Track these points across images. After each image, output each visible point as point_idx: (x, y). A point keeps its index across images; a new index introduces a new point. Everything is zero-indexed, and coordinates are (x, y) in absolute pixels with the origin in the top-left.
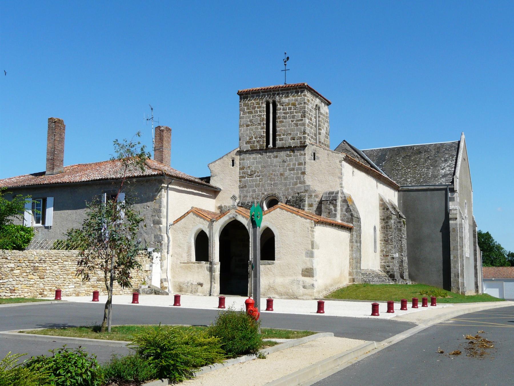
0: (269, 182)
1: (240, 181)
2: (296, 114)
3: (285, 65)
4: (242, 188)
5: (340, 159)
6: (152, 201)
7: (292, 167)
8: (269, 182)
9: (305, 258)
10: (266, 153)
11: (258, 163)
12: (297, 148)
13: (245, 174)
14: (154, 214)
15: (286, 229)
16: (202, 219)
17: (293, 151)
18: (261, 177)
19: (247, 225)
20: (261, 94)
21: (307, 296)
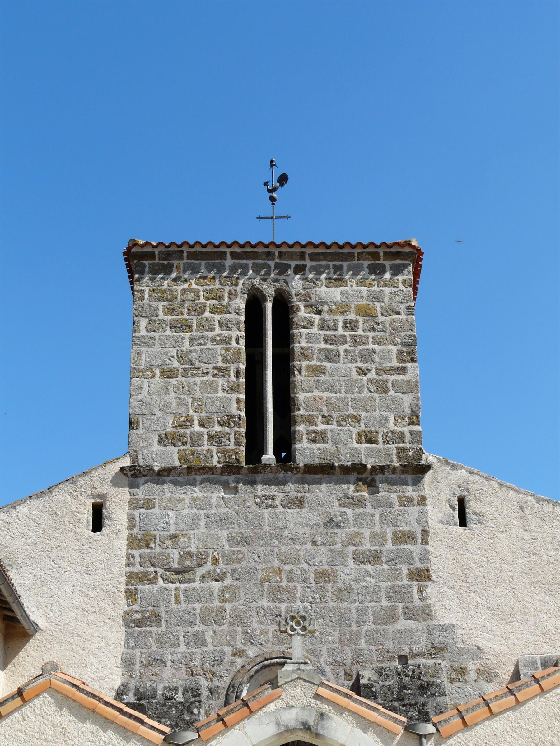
1: (131, 595)
2: (377, 348)
3: (273, 199)
4: (139, 623)
7: (367, 546)
8: (264, 603)
10: (253, 483)
11: (222, 522)
12: (388, 475)
13: (153, 565)
17: (372, 485)
18: (228, 581)
20: (229, 262)
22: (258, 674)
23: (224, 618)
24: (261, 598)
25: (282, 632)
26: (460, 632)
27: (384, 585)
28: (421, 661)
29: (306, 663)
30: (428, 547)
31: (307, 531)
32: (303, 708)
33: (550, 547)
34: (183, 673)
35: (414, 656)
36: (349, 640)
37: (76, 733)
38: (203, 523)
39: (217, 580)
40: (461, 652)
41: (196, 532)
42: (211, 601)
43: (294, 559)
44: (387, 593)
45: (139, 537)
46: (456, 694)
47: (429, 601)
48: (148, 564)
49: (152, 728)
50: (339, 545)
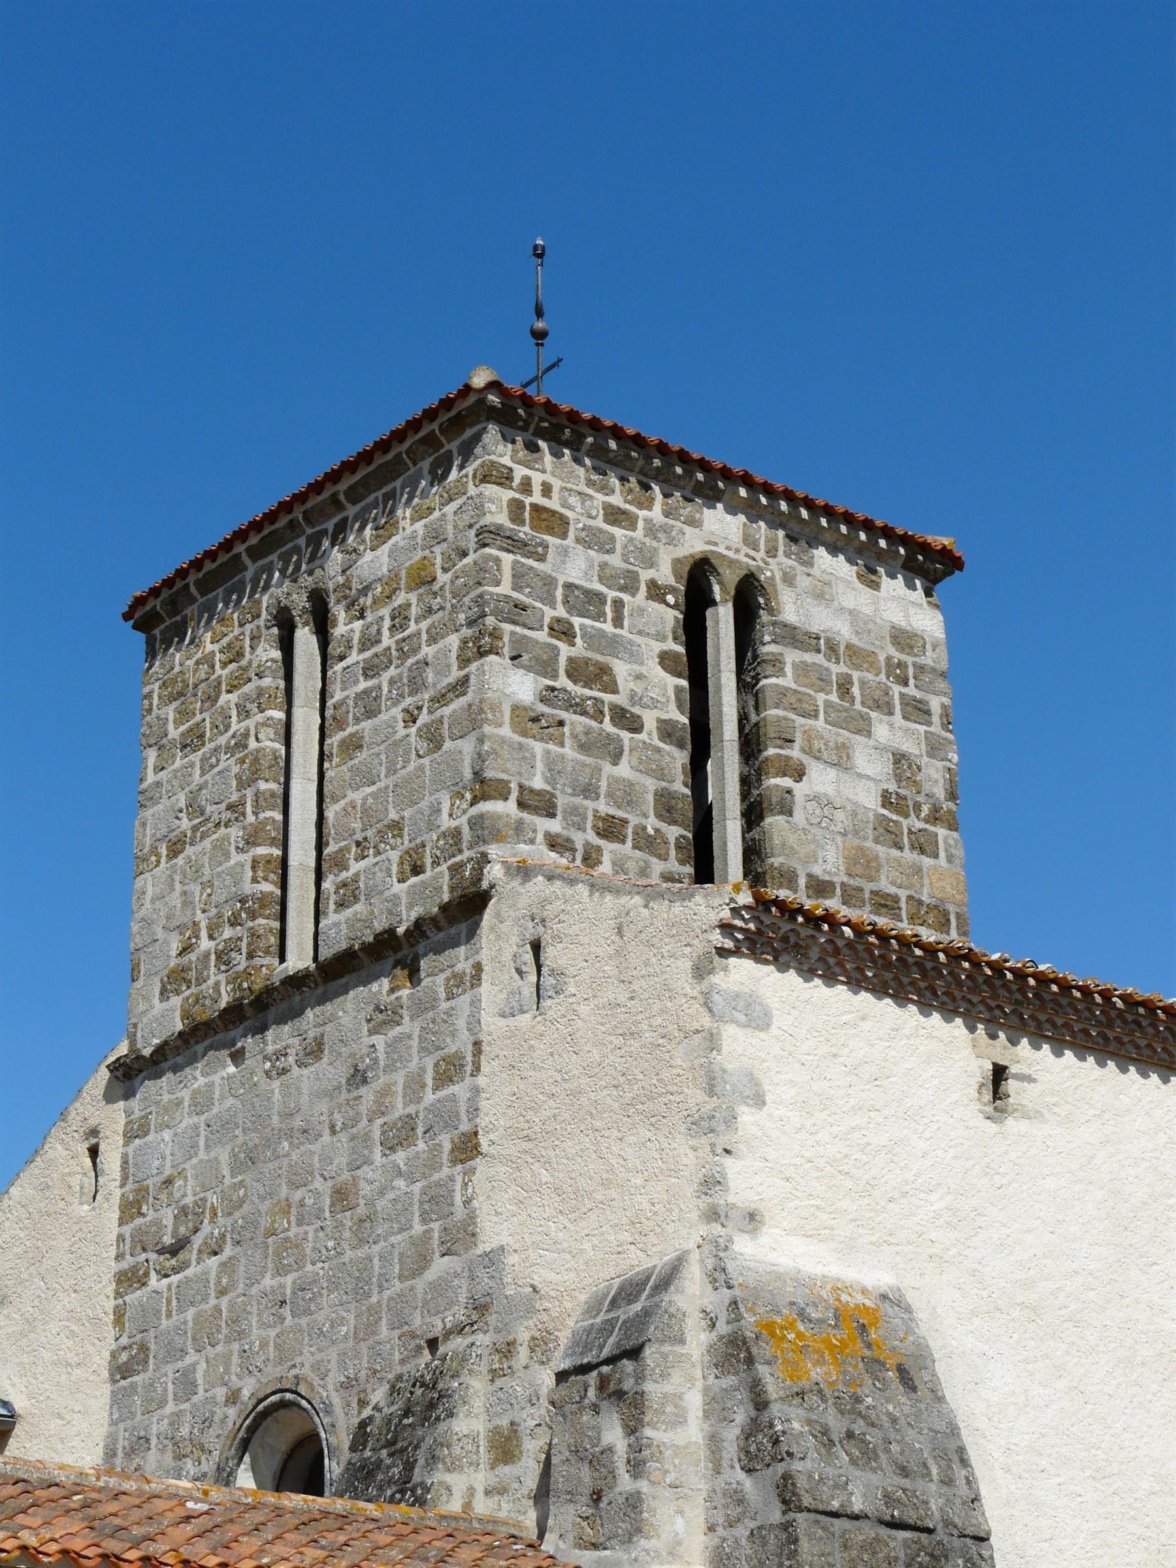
0: (268, 1282)
10: (262, 1029)
18: (228, 1251)
22: (258, 1434)
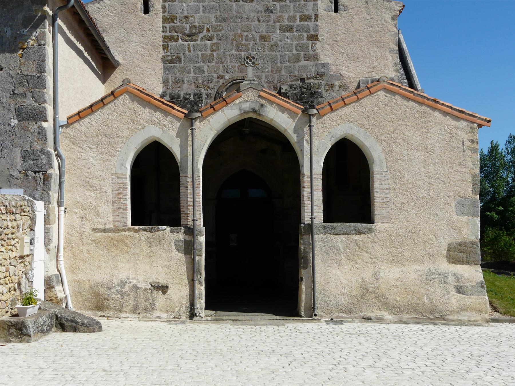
4: (170, 62)
5: (393, 13)
6: (14, 51)
7: (286, 23)
8: (234, 52)
9: (456, 217)
14: (20, 90)
15: (402, 143)
16: (158, 114)
18: (215, 41)
19: (295, 131)
21: (469, 314)
23: (213, 60)
24: (232, 49)
25: (242, 65)
26: (332, 67)
27: (295, 43)
28: (312, 81)
29: (254, 80)
30: (318, 23)
31: (256, 14)
32: (253, 102)
33: (380, 23)
34: (193, 87)
35: (308, 79)
36: (276, 71)
37: (141, 113)
38: (201, 10)
39: (209, 40)
40: (332, 76)
41: (198, 15)
42: (206, 51)
43: (249, 30)
44: (296, 47)
45: (168, 17)
46: (327, 97)
47: (317, 51)
48: (174, 31)
49: (178, 111)
50: (272, 22)
